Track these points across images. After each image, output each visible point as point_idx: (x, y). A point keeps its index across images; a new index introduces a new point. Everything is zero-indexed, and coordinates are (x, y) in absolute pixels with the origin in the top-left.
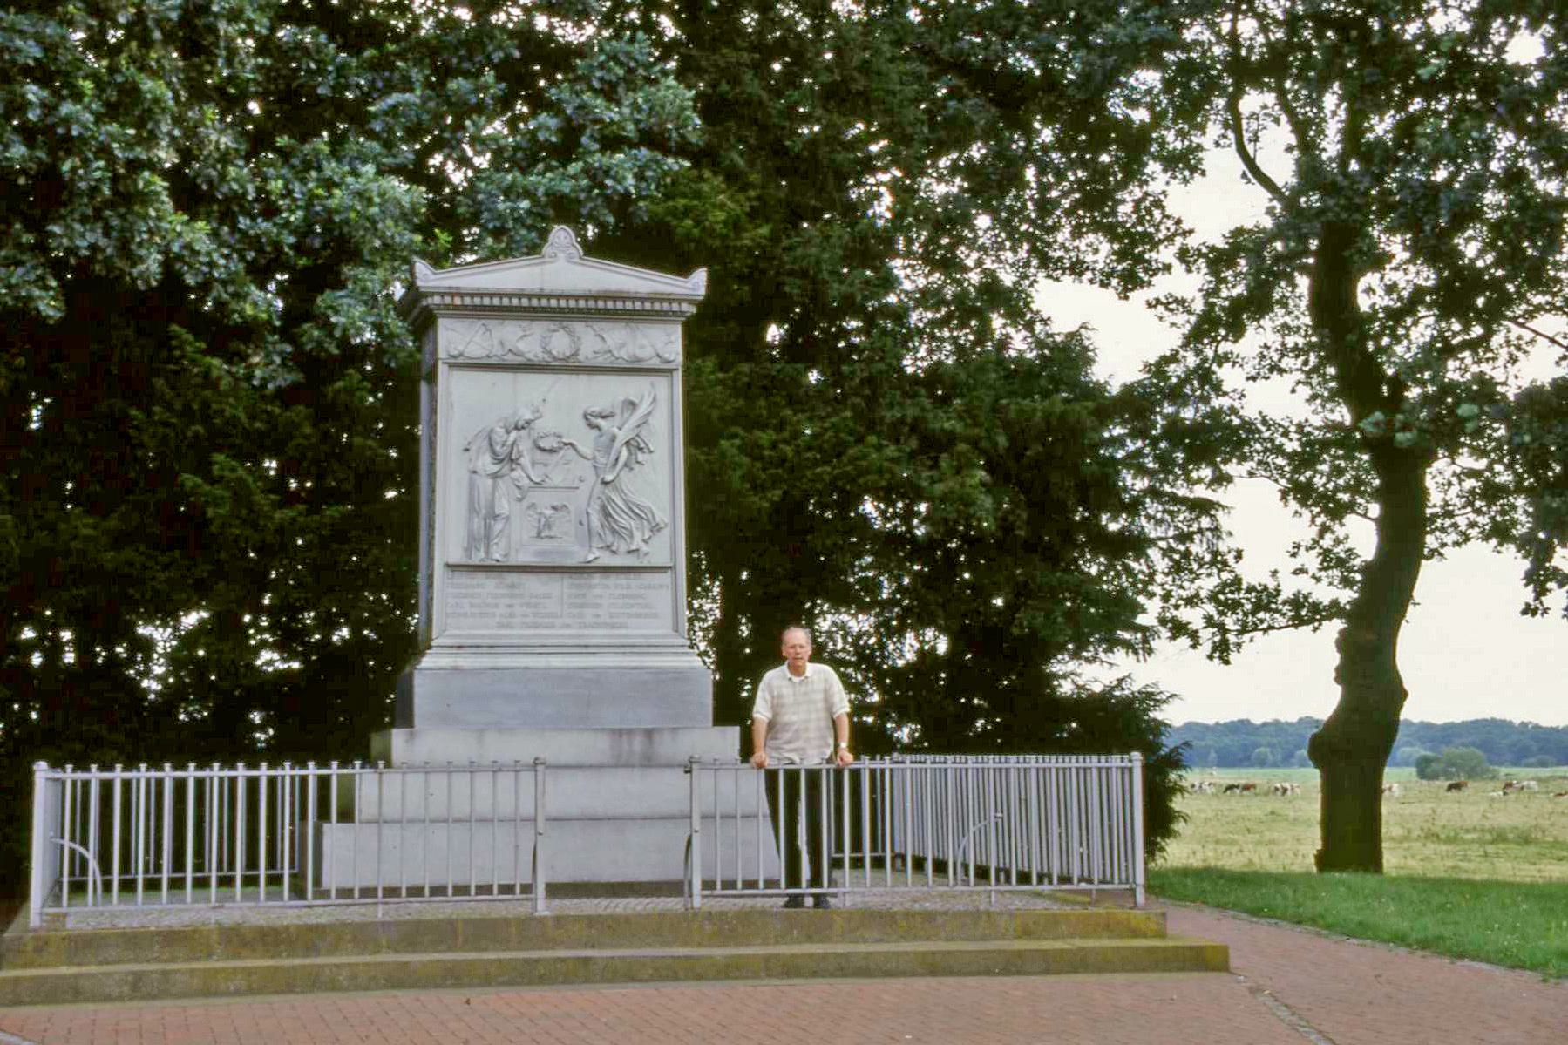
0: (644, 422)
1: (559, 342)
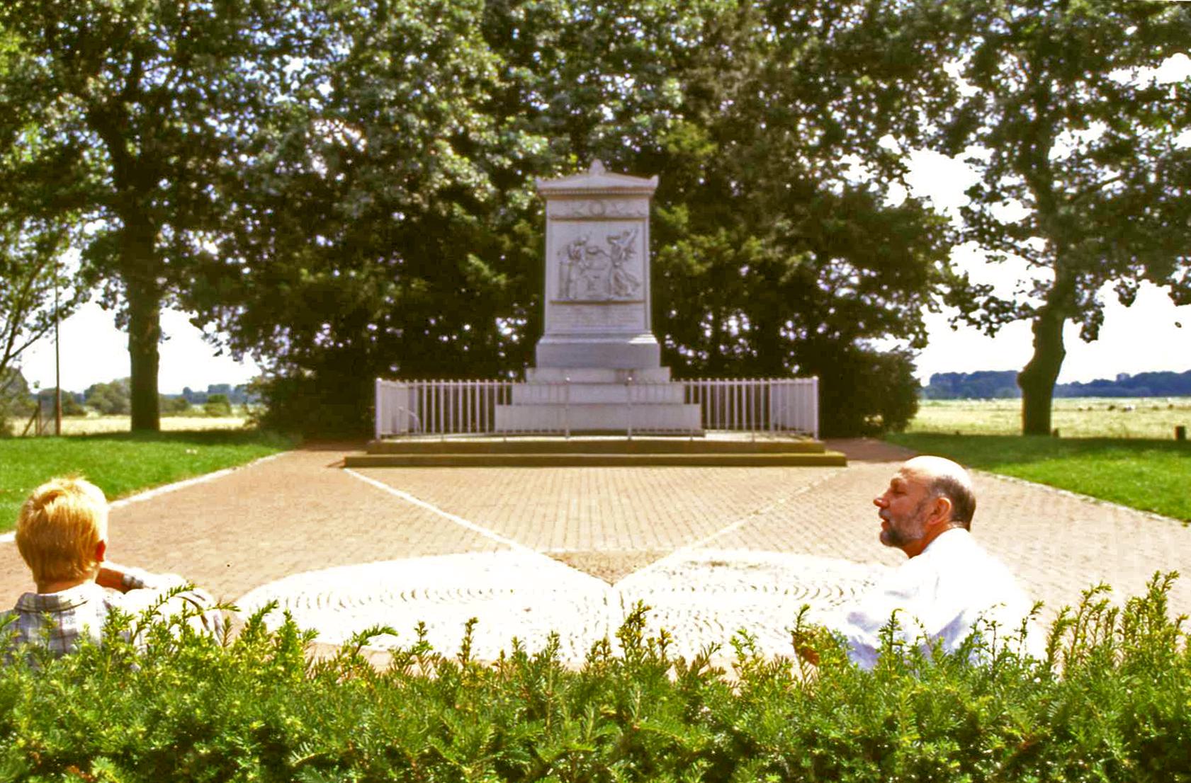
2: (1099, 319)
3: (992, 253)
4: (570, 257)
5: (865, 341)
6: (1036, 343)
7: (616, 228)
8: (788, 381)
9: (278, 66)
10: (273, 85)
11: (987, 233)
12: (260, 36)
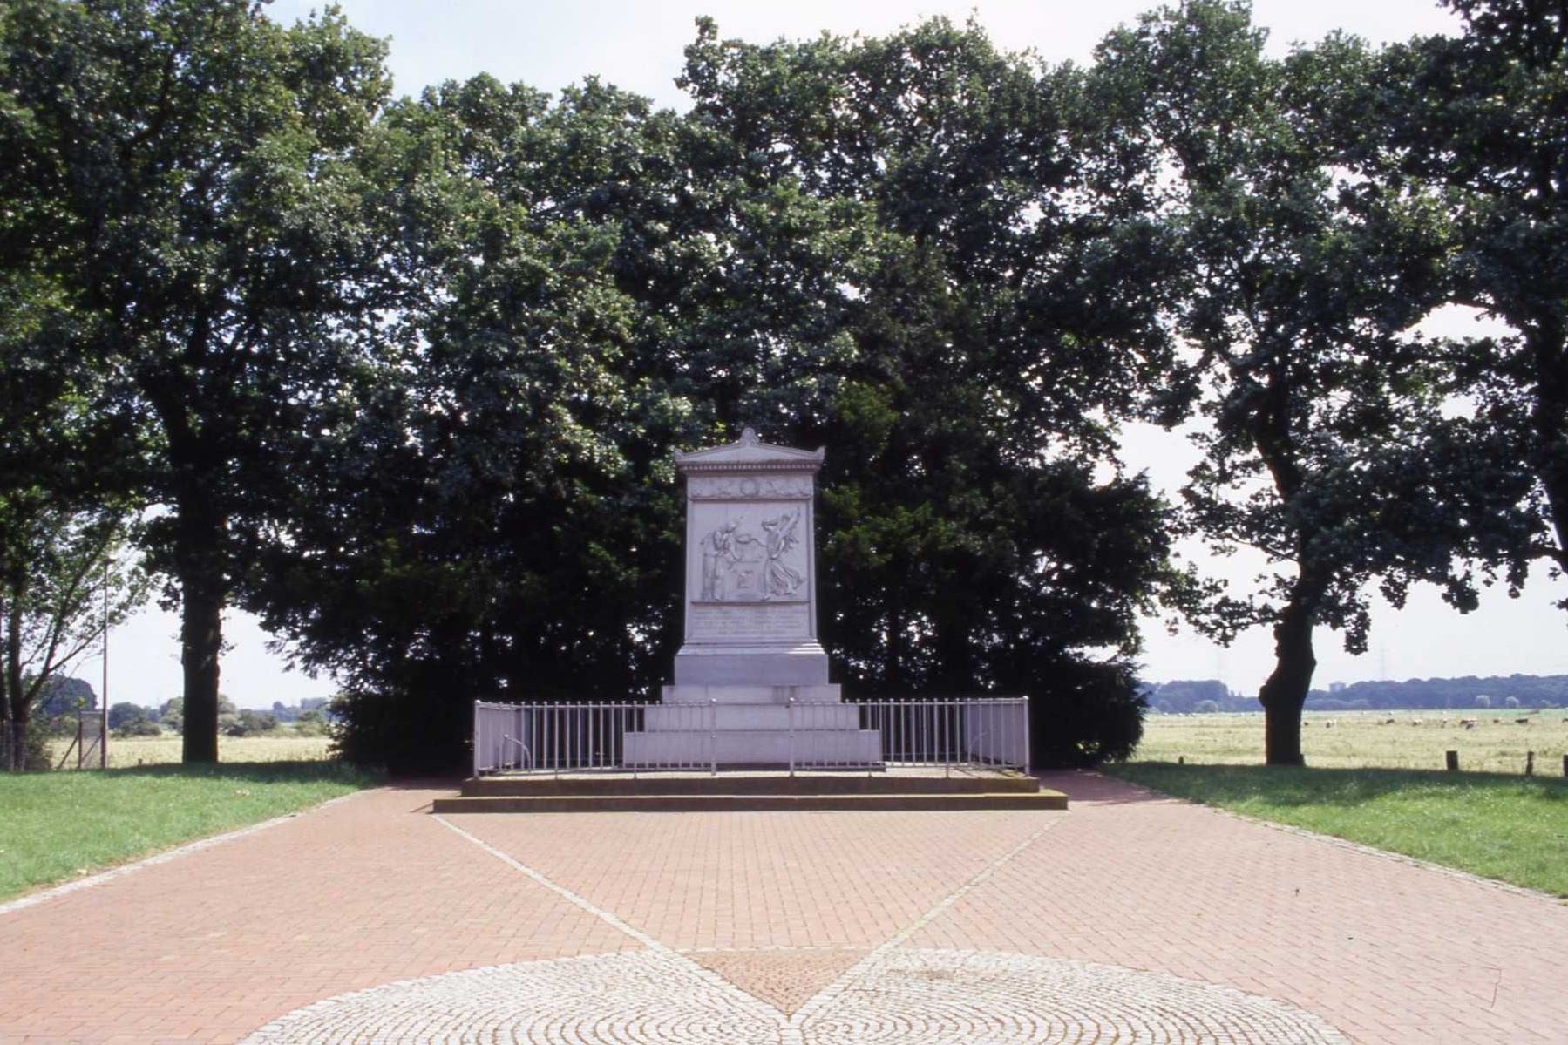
0: (794, 526)
1: (750, 487)
2: (1364, 622)
3: (1218, 542)
4: (716, 547)
5: (1077, 650)
6: (1280, 651)
7: (774, 511)
8: (982, 701)
9: (369, 322)
10: (362, 345)
11: (1215, 518)
12: (347, 285)
